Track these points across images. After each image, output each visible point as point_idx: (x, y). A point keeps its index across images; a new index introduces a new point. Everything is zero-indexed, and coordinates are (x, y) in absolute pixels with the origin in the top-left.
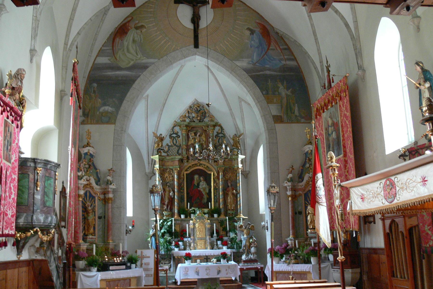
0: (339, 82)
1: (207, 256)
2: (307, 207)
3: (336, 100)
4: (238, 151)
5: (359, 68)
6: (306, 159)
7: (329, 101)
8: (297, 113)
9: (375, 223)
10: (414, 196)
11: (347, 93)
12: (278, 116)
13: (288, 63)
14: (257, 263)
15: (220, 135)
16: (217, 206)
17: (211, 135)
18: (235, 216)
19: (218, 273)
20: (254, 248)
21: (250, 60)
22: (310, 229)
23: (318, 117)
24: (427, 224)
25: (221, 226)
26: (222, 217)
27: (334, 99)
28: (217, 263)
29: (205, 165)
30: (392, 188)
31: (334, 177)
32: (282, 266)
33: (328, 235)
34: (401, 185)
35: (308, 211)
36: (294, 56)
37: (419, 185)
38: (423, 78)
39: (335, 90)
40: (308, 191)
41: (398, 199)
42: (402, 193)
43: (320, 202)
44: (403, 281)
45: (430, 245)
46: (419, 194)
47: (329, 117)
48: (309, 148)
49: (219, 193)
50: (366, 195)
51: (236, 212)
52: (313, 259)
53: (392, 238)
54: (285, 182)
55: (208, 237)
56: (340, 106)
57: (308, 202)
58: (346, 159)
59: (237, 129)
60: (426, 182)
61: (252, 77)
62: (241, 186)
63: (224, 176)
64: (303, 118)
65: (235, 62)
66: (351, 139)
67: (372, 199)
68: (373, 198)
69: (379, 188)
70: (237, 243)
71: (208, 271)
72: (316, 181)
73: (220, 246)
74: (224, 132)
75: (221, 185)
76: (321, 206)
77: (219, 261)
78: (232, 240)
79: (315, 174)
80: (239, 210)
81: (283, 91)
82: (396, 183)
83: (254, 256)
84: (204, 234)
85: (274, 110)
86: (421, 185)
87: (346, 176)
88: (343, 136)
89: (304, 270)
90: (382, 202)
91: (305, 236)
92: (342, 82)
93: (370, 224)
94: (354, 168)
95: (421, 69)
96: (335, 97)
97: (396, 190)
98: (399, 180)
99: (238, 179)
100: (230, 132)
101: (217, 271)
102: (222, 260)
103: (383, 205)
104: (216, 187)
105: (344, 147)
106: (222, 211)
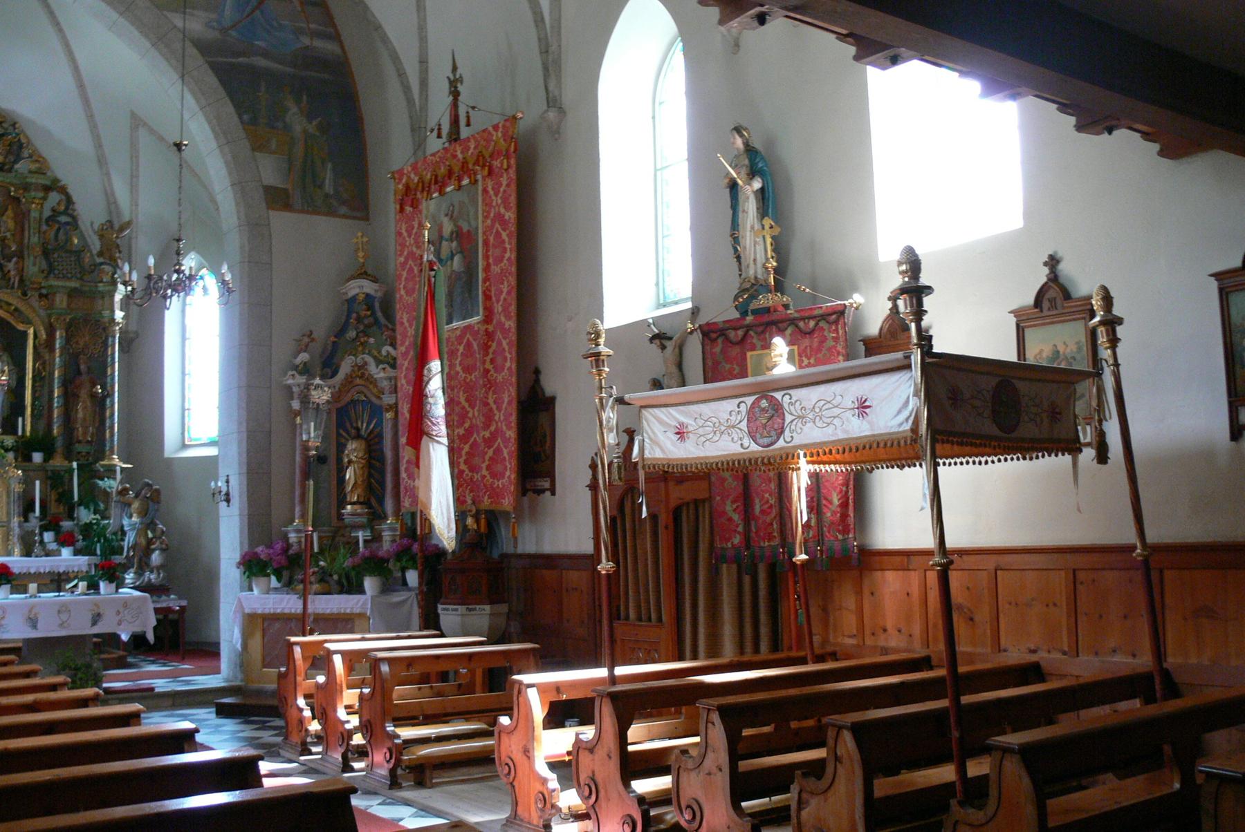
0: (491, 129)
1: (59, 574)
2: (345, 446)
3: (475, 174)
4: (115, 273)
5: (551, 104)
6: (348, 317)
7: (450, 173)
8: (328, 187)
9: (553, 494)
10: (832, 435)
11: (513, 161)
12: (276, 188)
13: (318, 43)
14: (168, 596)
15: (63, 219)
16: (42, 424)
17: (34, 214)
18: (96, 462)
19: (94, 623)
20: (160, 554)
21: (213, 16)
22: (351, 504)
23: (408, 209)
24: (731, 498)
25: (53, 487)
26: (58, 462)
27: (468, 170)
28: (86, 594)
29: (9, 304)
30: (773, 416)
31: (601, 380)
32: (282, 600)
33: (449, 519)
34: (799, 411)
35: (348, 455)
36: (334, 26)
37: (849, 414)
38: (747, 167)
39: (476, 147)
40: (349, 403)
41: (788, 439)
42: (801, 429)
43: (434, 433)
44: (646, 626)
45: (733, 545)
46: (846, 431)
47: (447, 215)
48: (360, 287)
49: (52, 392)
50: (691, 425)
51: (100, 450)
52: (369, 583)
53: (624, 531)
54: (290, 373)
55: (16, 521)
56: (485, 191)
57: (348, 433)
58: (491, 328)
59: (113, 207)
60: (867, 410)
61: (217, 69)
62: (117, 373)
63: (68, 340)
64: (344, 203)
65: (169, 15)
66: (513, 280)
67: (710, 436)
68: (715, 433)
69: (733, 413)
70: (106, 539)
71: (64, 617)
72: (426, 379)
73: (53, 546)
74: (74, 210)
75: (57, 366)
76: (435, 444)
77: (93, 587)
78: (87, 529)
79: (422, 360)
80: (108, 445)
81: (297, 122)
82: (786, 405)
83: (159, 574)
84: (5, 512)
85: (270, 171)
86: (853, 415)
87: (487, 371)
88: (487, 269)
89: (348, 611)
90: (742, 444)
91: (335, 522)
92: (500, 130)
93: (539, 495)
94: (514, 354)
95: (744, 143)
96: (470, 166)
97: (784, 419)
98: (796, 402)
99: (109, 353)
100: (90, 213)
101: (91, 617)
102: (102, 585)
103: (742, 451)
104: (40, 373)
105: (487, 297)
106: (59, 444)
